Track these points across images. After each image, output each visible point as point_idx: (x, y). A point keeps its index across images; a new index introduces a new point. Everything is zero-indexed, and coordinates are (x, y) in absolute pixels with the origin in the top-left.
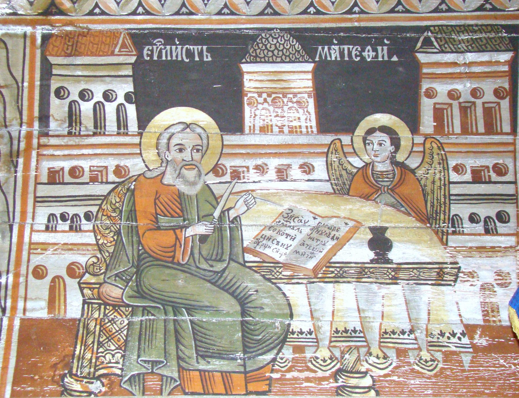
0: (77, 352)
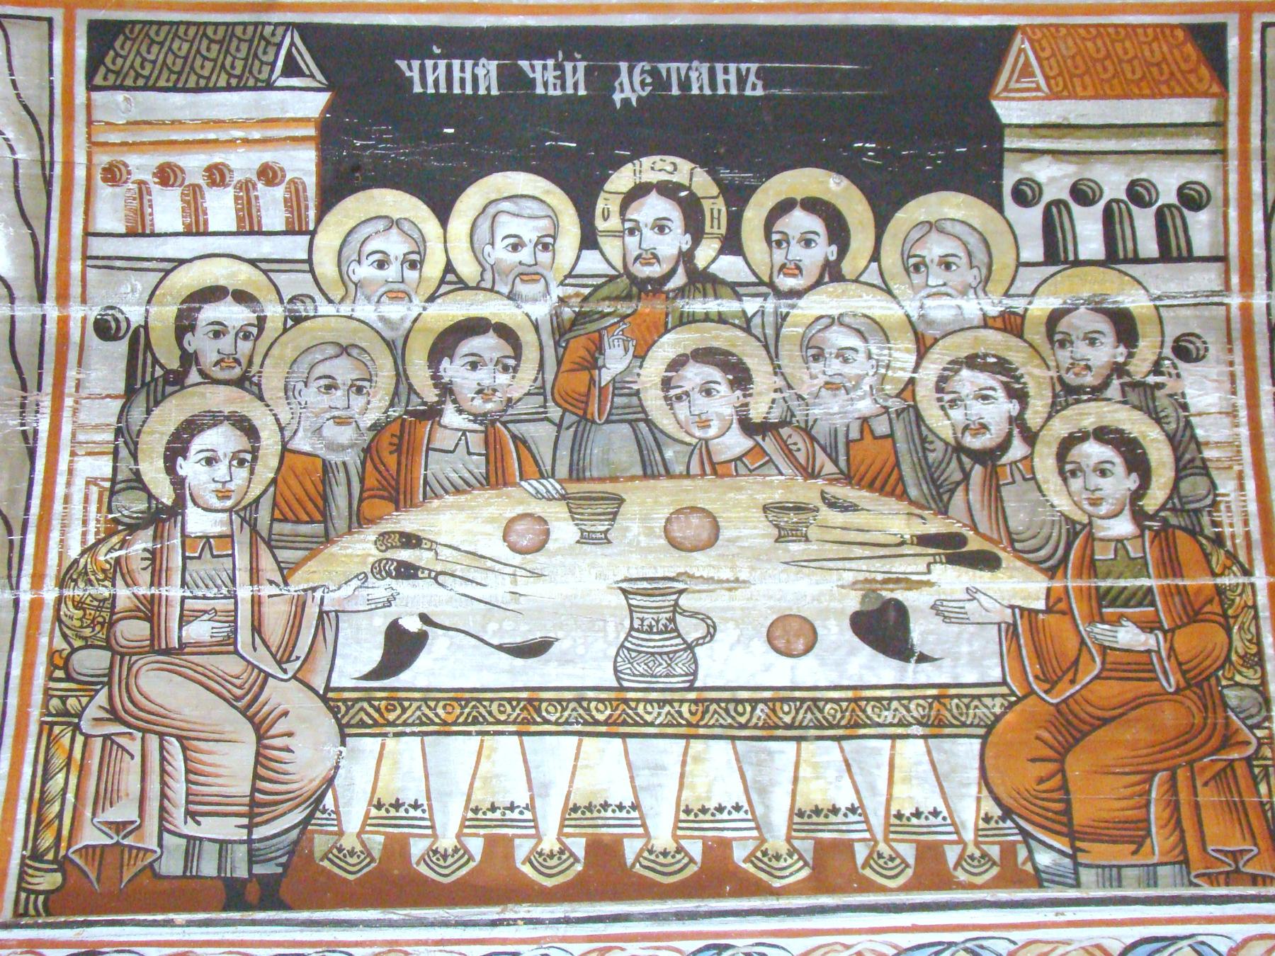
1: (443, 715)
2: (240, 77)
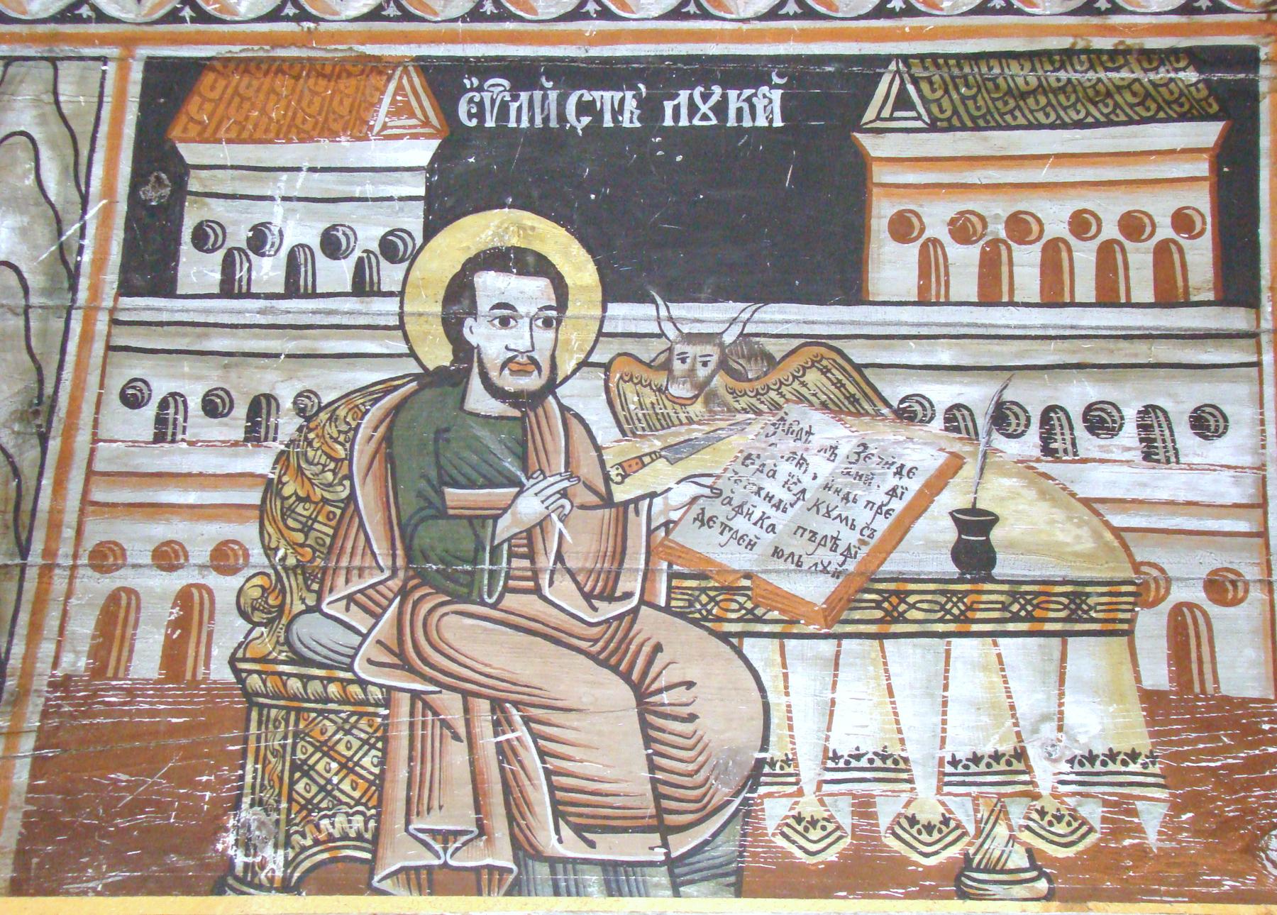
0: (249, 779)
1: (327, 723)
2: (949, 120)
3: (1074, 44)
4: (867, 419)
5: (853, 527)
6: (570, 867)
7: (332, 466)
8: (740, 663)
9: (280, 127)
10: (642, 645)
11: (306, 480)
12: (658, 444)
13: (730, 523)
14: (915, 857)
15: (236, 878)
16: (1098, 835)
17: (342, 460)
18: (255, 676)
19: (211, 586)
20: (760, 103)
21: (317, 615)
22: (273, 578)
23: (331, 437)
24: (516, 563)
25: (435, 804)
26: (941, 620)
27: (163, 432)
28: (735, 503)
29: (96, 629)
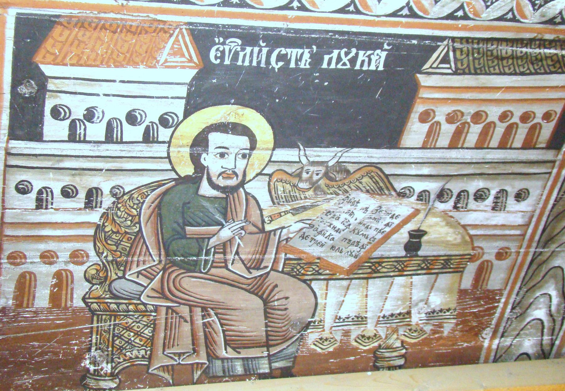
0: (94, 341)
2: (464, 70)
3: (537, 36)
4: (385, 196)
5: (367, 238)
6: (230, 361)
7: (130, 218)
8: (310, 290)
9: (103, 59)
10: (269, 285)
11: (117, 225)
12: (289, 208)
13: (315, 238)
14: (361, 347)
15: (91, 374)
16: (427, 335)
17: (135, 216)
18: (95, 304)
19: (71, 270)
20: (374, 58)
21: (123, 280)
22: (102, 266)
23: (130, 206)
24: (217, 256)
25: (176, 344)
26: (394, 271)
27: (40, 204)
28: (319, 230)
29: (15, 288)
